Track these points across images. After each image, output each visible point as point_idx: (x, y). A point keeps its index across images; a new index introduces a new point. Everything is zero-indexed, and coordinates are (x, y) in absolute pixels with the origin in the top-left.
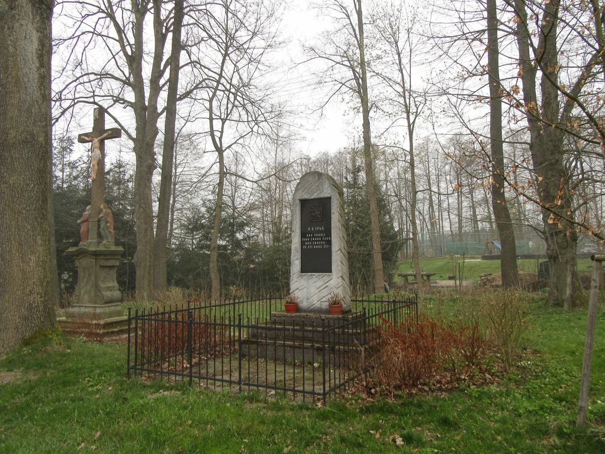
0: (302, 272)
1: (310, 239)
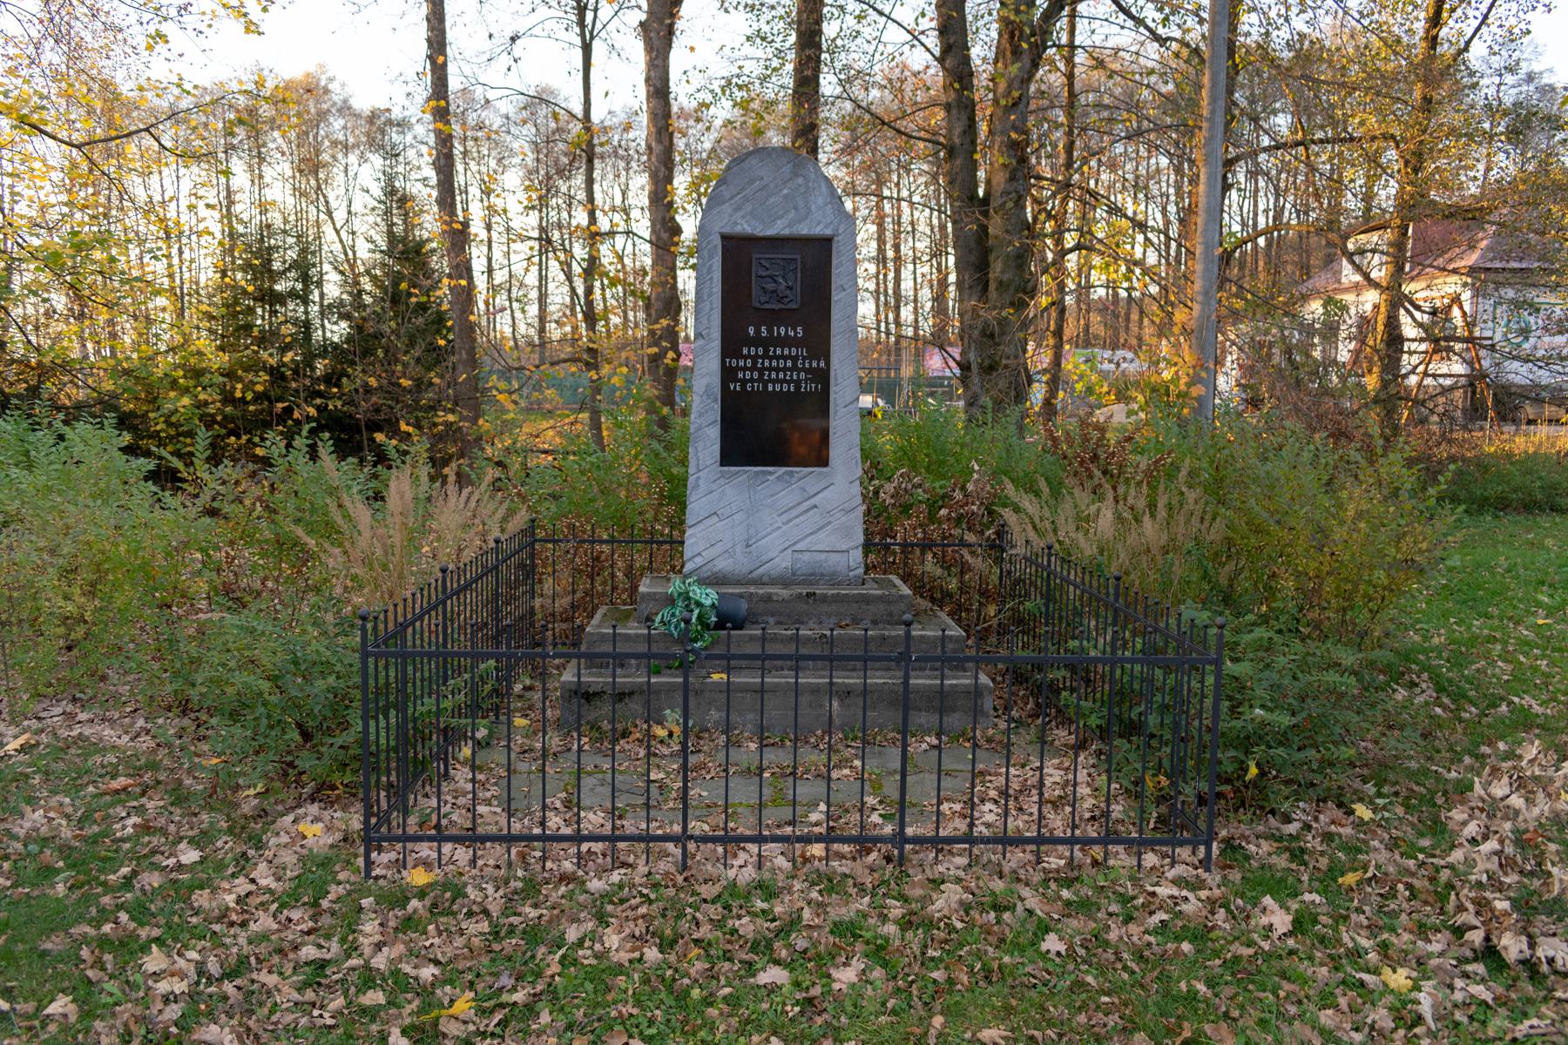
0: (722, 465)
1: (755, 363)
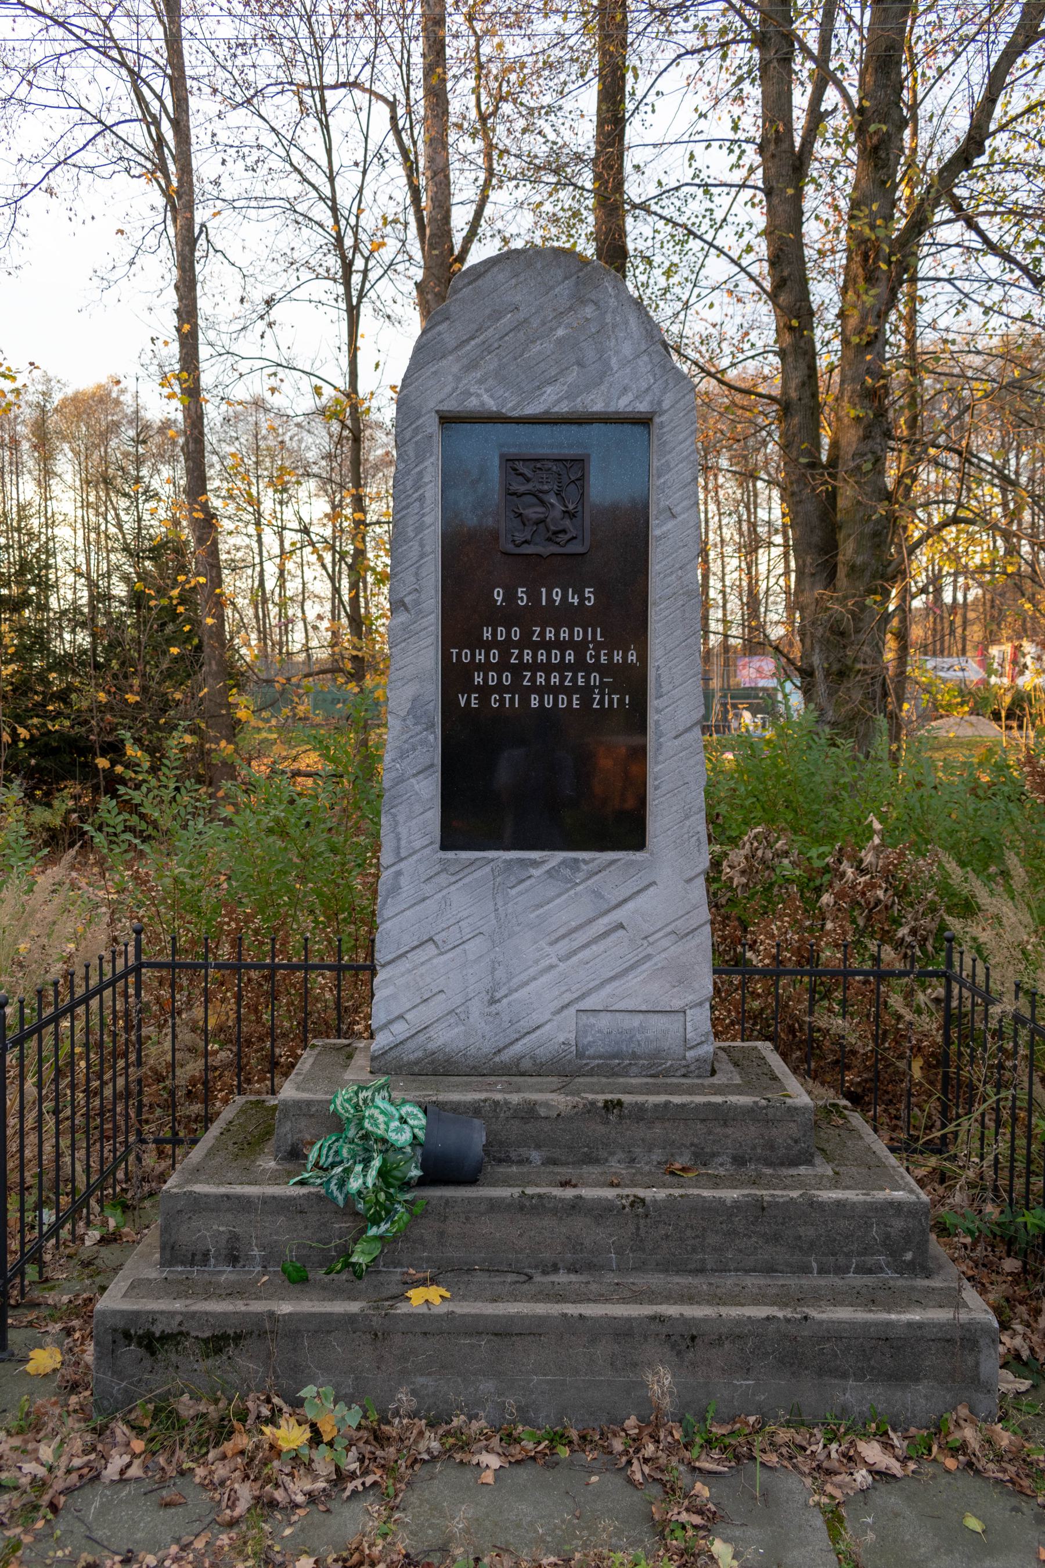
0: (444, 847)
1: (505, 655)
